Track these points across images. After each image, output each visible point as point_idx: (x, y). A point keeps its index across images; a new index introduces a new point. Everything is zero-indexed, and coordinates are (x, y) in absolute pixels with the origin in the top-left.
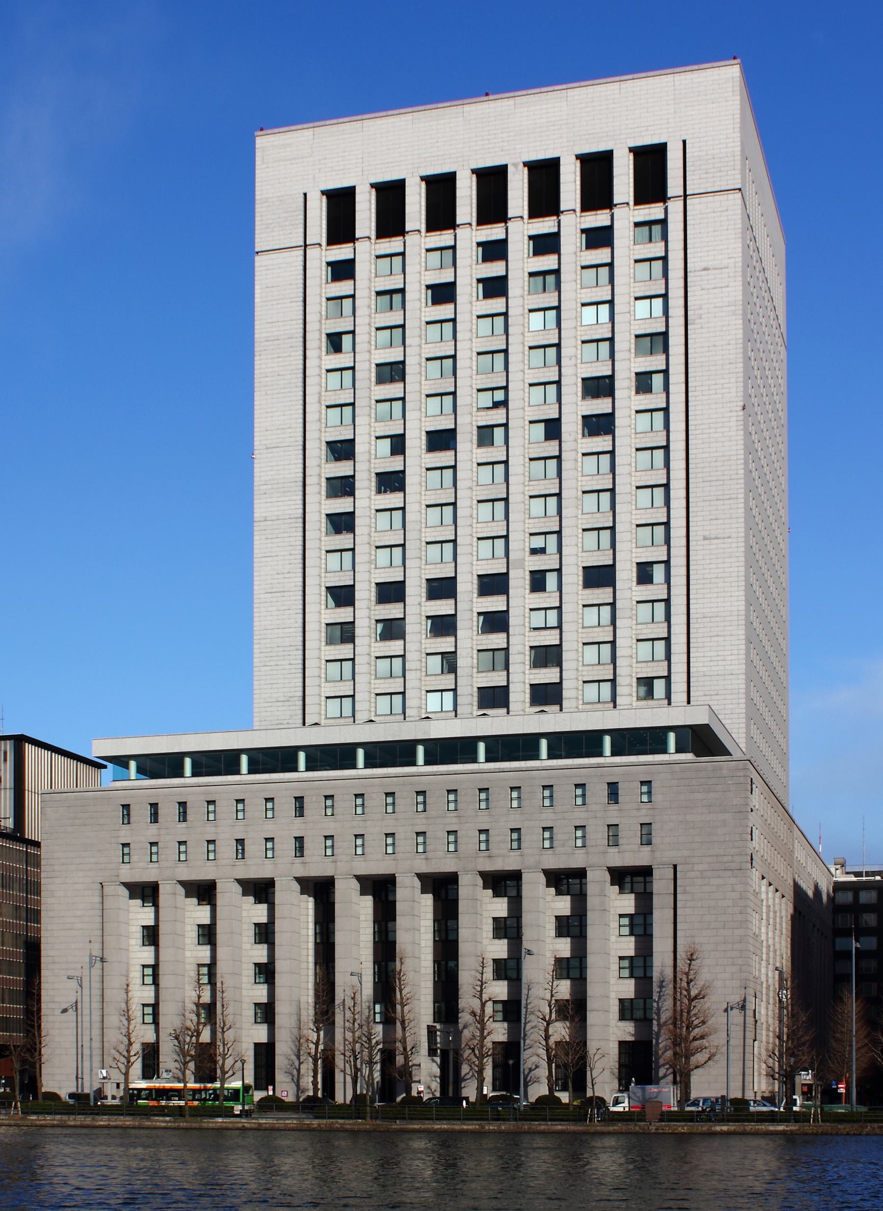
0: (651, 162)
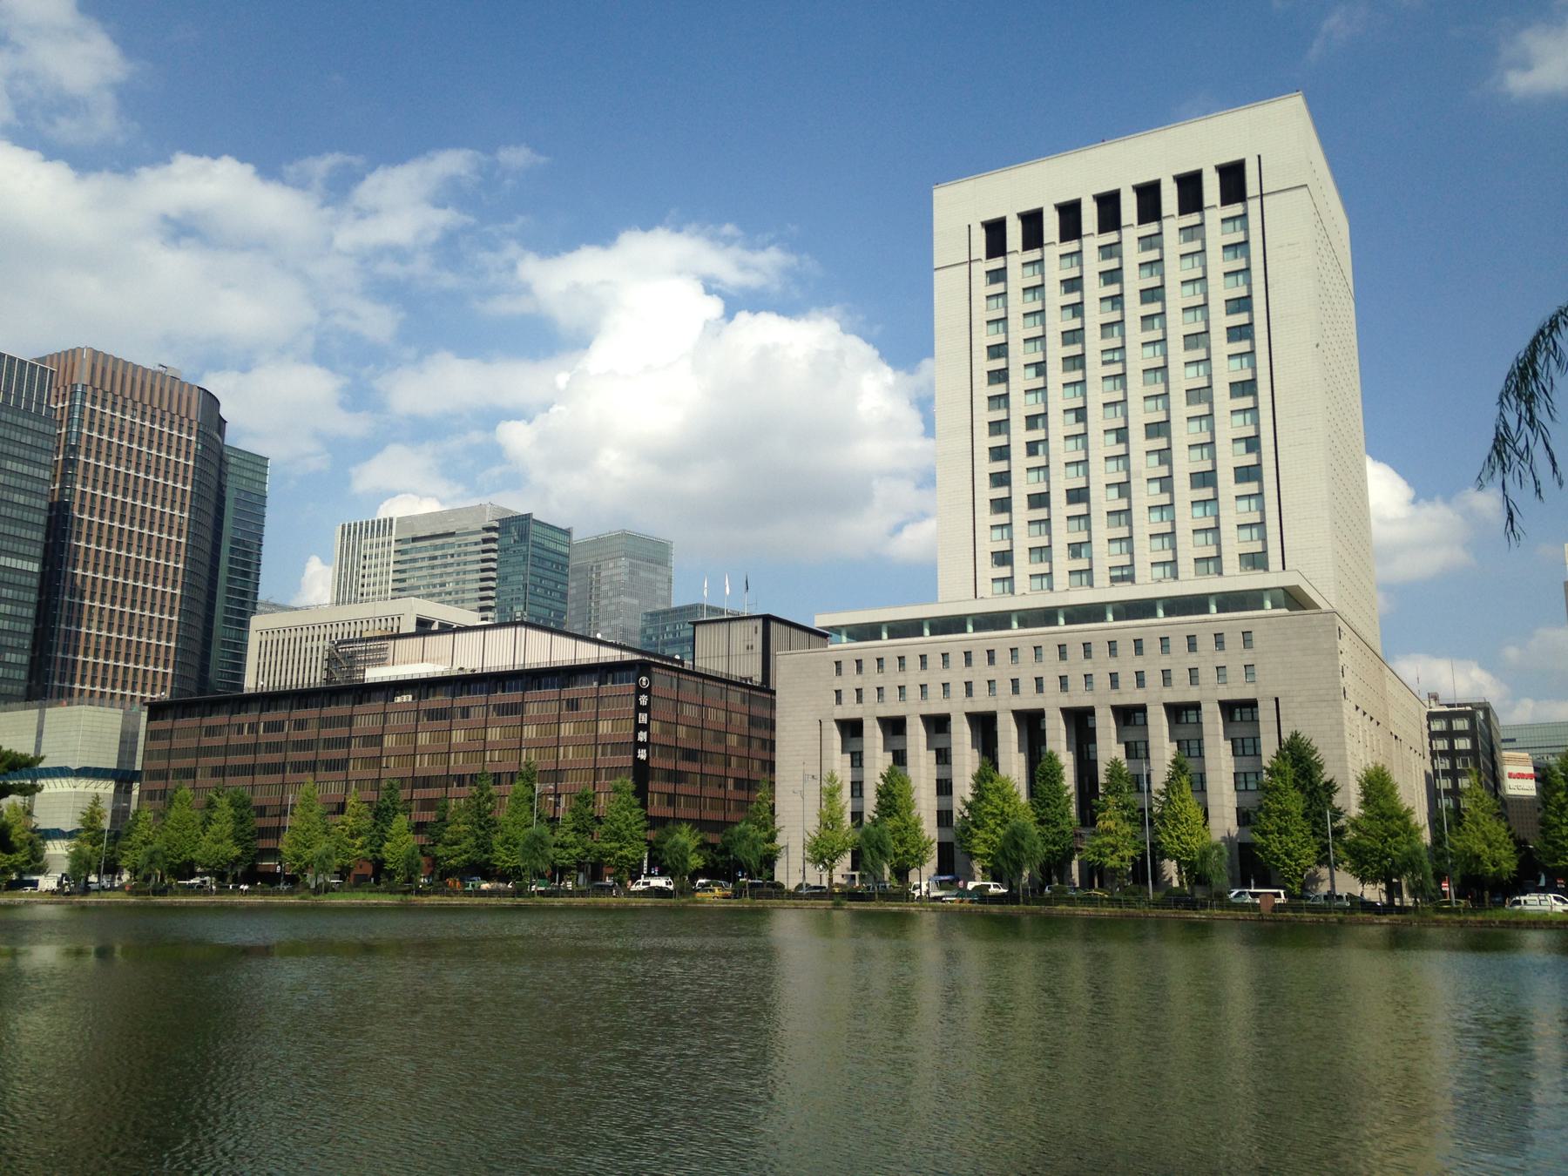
0: (1233, 178)
